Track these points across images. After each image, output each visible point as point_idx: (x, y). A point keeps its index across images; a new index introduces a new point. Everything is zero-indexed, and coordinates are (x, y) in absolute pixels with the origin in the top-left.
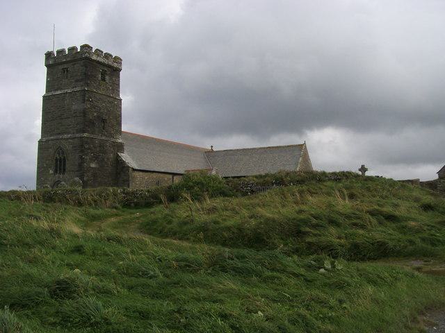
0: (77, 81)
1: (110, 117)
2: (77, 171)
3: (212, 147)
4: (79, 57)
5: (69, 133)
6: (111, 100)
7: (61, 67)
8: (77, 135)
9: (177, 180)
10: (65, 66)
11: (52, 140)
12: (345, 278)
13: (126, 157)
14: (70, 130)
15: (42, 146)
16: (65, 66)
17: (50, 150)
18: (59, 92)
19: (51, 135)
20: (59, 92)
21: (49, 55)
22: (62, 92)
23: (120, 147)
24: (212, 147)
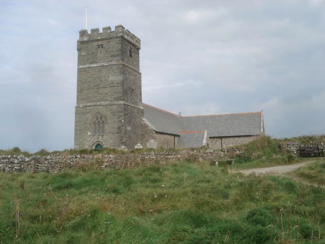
0: (113, 56)
1: (130, 88)
2: (117, 133)
3: (180, 113)
4: (115, 36)
5: (107, 100)
6: (136, 73)
7: (95, 44)
8: (115, 103)
9: (247, 141)
10: (100, 43)
11: (90, 106)
12: (171, 217)
13: (146, 121)
14: (107, 98)
15: (79, 112)
16: (100, 43)
17: (88, 115)
18: (95, 65)
19: (88, 102)
20: (95, 65)
21: (83, 33)
22: (99, 65)
23: (142, 112)
24: (180, 113)
